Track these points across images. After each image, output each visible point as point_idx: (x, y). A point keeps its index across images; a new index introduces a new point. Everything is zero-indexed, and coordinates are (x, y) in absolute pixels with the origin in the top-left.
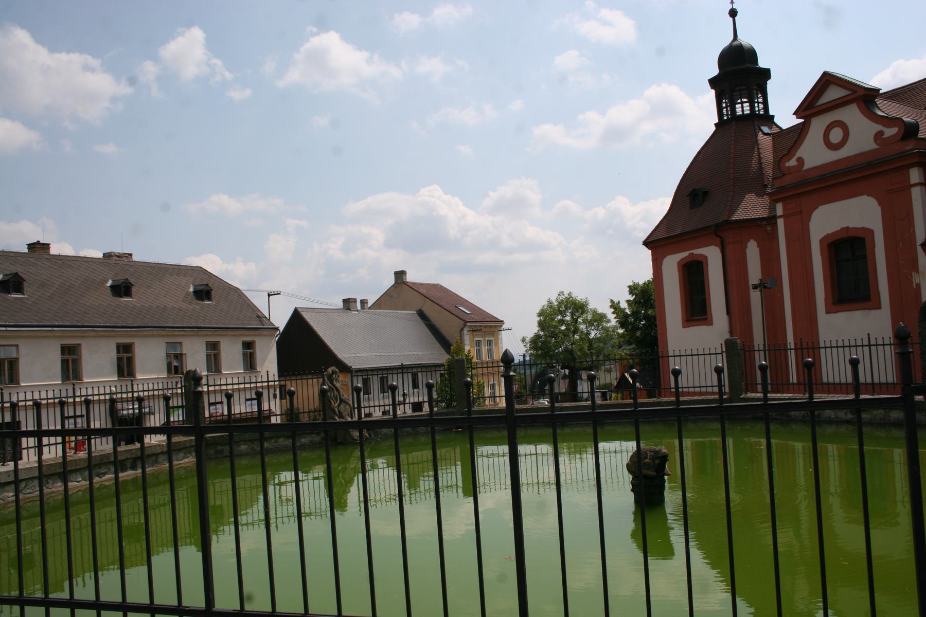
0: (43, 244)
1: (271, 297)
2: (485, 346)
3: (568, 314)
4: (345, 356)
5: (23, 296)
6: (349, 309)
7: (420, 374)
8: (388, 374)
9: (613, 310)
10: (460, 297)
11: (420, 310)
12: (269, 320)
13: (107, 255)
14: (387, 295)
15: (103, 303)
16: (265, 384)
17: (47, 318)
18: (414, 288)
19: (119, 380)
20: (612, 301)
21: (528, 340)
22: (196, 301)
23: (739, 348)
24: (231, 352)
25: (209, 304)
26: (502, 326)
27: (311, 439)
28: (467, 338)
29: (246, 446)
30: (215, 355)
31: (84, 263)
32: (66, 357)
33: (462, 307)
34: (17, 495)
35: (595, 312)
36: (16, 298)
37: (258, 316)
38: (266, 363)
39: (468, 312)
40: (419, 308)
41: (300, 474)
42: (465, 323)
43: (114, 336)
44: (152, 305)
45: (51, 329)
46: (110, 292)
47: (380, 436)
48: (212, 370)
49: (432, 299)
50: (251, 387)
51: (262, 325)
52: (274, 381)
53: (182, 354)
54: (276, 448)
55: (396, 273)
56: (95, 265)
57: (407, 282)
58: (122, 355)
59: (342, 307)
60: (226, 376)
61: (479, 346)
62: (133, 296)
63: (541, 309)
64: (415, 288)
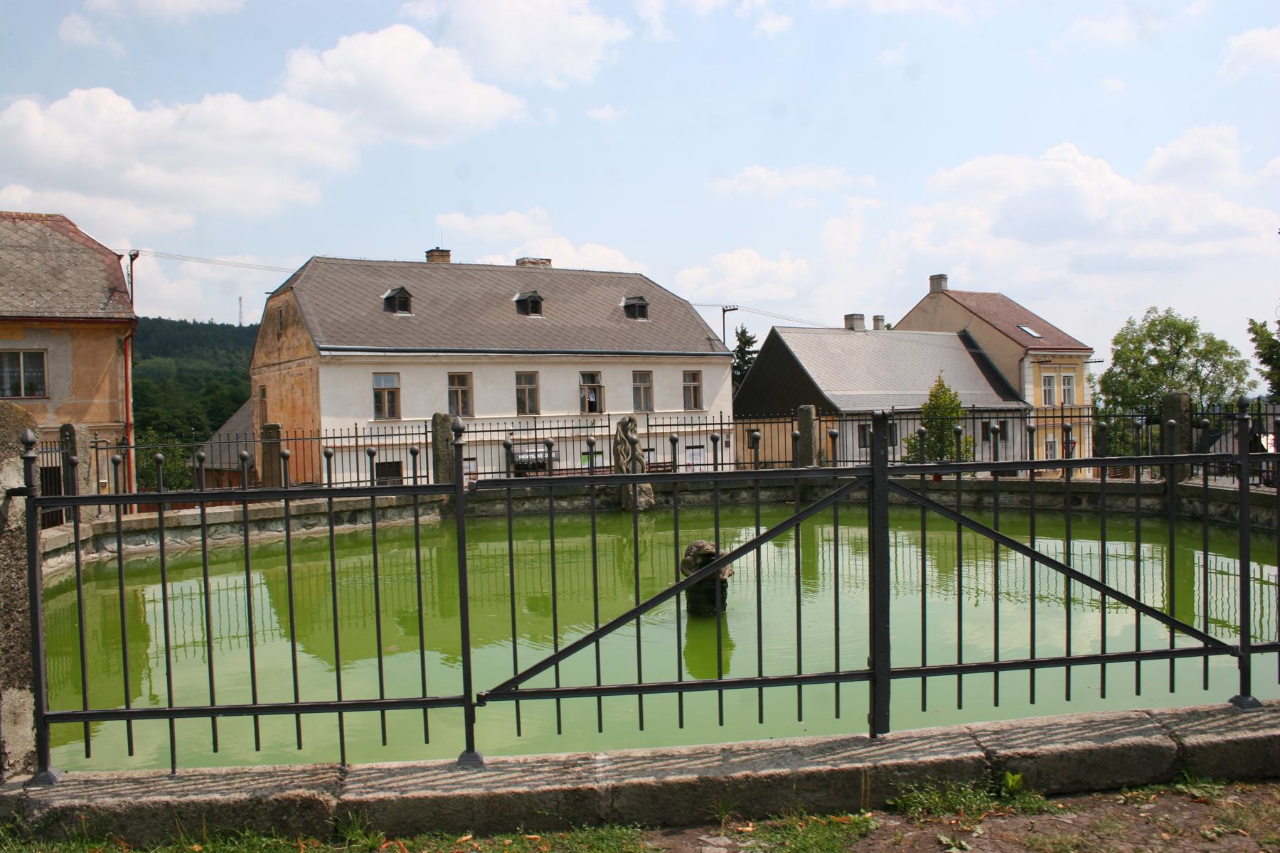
0: (442, 251)
3: (1165, 341)
4: (835, 393)
5: (409, 315)
6: (852, 329)
7: (1010, 421)
8: (990, 418)
9: (1254, 336)
10: (1030, 312)
11: (964, 331)
13: (520, 262)
14: (919, 308)
15: (503, 322)
16: (718, 427)
17: (433, 341)
18: (957, 299)
19: (375, 422)
20: (1252, 322)
21: (1097, 378)
22: (625, 318)
23: (1184, 409)
24: (668, 383)
25: (642, 323)
26: (1090, 356)
28: (1029, 371)
30: (695, 388)
31: (488, 272)
34: (204, 540)
35: (1210, 340)
36: (402, 318)
37: (709, 339)
38: (717, 401)
39: (1035, 334)
41: (1254, 566)
42: (1027, 350)
43: (513, 364)
44: (566, 324)
45: (382, 354)
46: (515, 308)
49: (982, 316)
51: (710, 349)
53: (600, 387)
54: (541, 510)
55: (933, 279)
56: (501, 274)
57: (947, 291)
58: (523, 386)
60: (544, 419)
62: (543, 313)
63: (1119, 334)
64: (958, 300)
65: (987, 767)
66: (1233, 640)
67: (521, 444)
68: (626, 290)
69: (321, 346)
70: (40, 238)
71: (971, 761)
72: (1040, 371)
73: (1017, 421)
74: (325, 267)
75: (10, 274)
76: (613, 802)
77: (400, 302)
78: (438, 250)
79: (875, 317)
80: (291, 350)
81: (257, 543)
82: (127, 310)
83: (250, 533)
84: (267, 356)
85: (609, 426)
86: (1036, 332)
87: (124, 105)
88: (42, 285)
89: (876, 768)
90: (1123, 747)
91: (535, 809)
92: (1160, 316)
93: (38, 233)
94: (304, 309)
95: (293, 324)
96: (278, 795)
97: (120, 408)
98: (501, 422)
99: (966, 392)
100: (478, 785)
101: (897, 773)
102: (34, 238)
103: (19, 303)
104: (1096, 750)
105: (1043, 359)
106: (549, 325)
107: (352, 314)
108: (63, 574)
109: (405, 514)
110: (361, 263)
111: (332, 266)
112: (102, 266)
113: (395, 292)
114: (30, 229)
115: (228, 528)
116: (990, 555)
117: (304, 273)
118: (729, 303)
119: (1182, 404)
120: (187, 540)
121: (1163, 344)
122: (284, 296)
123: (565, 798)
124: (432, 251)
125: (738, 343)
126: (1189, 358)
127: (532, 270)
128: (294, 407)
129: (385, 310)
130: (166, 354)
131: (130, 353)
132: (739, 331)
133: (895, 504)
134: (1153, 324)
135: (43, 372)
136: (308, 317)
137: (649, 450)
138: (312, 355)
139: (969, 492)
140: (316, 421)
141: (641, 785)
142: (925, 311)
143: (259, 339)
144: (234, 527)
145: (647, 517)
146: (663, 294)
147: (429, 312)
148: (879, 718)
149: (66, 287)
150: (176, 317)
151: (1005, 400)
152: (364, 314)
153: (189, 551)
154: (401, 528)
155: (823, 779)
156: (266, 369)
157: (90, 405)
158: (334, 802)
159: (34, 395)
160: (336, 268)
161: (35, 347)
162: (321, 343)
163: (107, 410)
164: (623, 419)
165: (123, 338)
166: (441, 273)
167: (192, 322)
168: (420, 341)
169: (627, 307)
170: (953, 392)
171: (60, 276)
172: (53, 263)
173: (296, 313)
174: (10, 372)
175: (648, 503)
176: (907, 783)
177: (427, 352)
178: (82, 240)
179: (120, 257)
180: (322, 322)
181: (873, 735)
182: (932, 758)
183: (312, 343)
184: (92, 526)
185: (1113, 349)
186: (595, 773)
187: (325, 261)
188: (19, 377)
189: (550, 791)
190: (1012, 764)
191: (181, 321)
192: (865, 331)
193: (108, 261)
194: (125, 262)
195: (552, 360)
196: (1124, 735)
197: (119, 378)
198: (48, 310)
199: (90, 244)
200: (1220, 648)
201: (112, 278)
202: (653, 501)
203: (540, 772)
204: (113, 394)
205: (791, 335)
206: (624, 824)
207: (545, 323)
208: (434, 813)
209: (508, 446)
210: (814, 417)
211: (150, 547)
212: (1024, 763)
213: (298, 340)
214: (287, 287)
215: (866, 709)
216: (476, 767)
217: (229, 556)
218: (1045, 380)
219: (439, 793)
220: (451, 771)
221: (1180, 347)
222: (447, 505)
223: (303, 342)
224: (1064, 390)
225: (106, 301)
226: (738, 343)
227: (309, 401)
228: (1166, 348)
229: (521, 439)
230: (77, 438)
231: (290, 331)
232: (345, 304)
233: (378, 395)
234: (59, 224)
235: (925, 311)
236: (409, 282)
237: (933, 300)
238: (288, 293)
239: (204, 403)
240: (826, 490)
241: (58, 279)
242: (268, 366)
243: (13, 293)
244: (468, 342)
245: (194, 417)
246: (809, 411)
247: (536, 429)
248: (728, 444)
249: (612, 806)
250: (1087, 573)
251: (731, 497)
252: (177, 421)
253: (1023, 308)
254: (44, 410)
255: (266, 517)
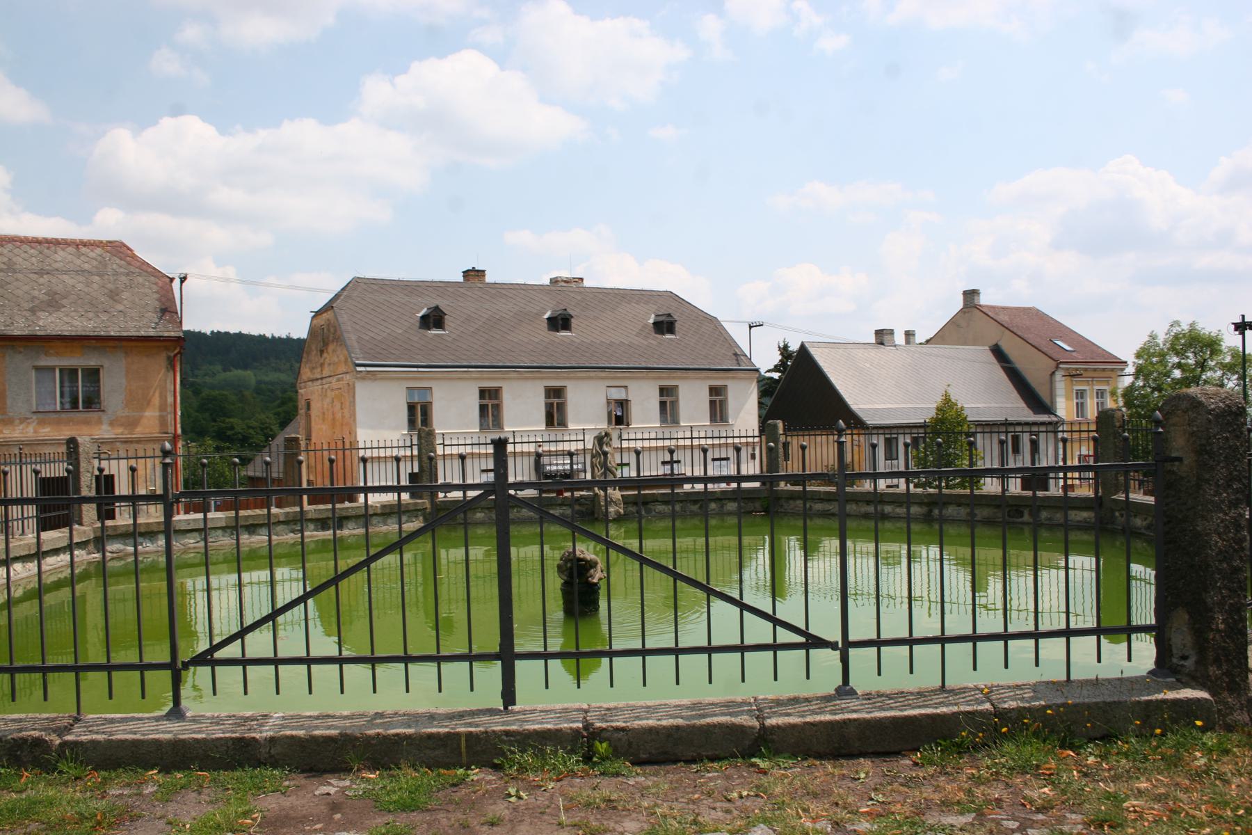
0: (478, 271)
1: (753, 329)
2: (1092, 398)
4: (862, 407)
5: (443, 332)
6: (882, 344)
8: (898, 434)
10: (1064, 326)
12: (750, 359)
14: (953, 322)
15: (533, 339)
17: (464, 357)
18: (990, 314)
19: (546, 430)
22: (654, 334)
23: (1118, 424)
25: (670, 339)
26: (1124, 369)
27: (561, 511)
28: (1061, 384)
29: (483, 514)
31: (520, 291)
32: (714, 398)
33: (1062, 341)
36: (435, 335)
37: (736, 354)
39: (1068, 348)
40: (994, 343)
46: (546, 325)
47: (654, 513)
48: (488, 425)
49: (1015, 330)
50: (720, 444)
51: (740, 365)
52: (754, 437)
54: (518, 518)
56: (534, 293)
57: (980, 306)
59: (874, 342)
61: (1102, 397)
64: (992, 315)
65: (584, 737)
66: (836, 636)
67: (550, 455)
68: (656, 307)
69: (357, 362)
70: (100, 262)
71: (569, 731)
72: (1072, 385)
73: (1051, 435)
74: (365, 287)
75: (72, 296)
76: (270, 749)
77: (434, 320)
78: (474, 270)
79: (906, 331)
80: (332, 366)
81: (247, 546)
82: (176, 329)
83: (241, 537)
84: (311, 371)
85: (584, 440)
86: (1069, 345)
87: (209, 131)
88: (100, 307)
89: (486, 732)
90: (708, 725)
91: (210, 753)
92: (1183, 330)
93: (99, 258)
94: (343, 327)
95: (333, 341)
96: (15, 735)
97: (169, 420)
98: (468, 437)
99: (997, 405)
100: (169, 732)
101: (505, 738)
102: (95, 263)
103: (78, 323)
104: (683, 727)
105: (1074, 373)
106: (578, 341)
107: (389, 331)
108: (62, 571)
109: (389, 521)
110: (400, 283)
111: (372, 286)
112: (155, 288)
113: (430, 311)
114: (92, 254)
115: (220, 532)
116: (1000, 573)
117: (345, 293)
118: (755, 319)
119: (1116, 420)
120: (182, 542)
121: (1188, 357)
122: (325, 314)
123: (233, 744)
124: (468, 271)
125: (780, 357)
126: (1215, 372)
127: (565, 289)
128: (334, 419)
129: (420, 328)
130: (245, 367)
131: (178, 369)
132: (782, 345)
133: (891, 517)
134: (1176, 337)
135: (99, 387)
136: (346, 335)
137: (622, 465)
138: (349, 371)
139: (921, 504)
140: (352, 433)
141: (292, 737)
142: (958, 326)
143: (305, 355)
144: (226, 532)
145: (616, 526)
146: (692, 311)
147: (462, 329)
148: (509, 695)
149: (120, 307)
150: (255, 332)
151: (1035, 413)
152: (400, 331)
153: (182, 553)
154: (386, 534)
155: (441, 739)
156: (310, 383)
157: (141, 417)
158: (58, 742)
159: (91, 408)
160: (376, 287)
161: (92, 363)
162: (358, 359)
163: (157, 422)
164: (600, 433)
165: (172, 354)
166: (476, 292)
167: (270, 337)
168: (453, 357)
169: (655, 324)
170: (959, 406)
171: (116, 298)
172: (110, 286)
173: (335, 331)
174: (69, 387)
175: (617, 513)
176: (510, 746)
177: (458, 368)
178: (138, 264)
179: (172, 280)
180: (359, 339)
181: (506, 708)
182: (537, 727)
183: (349, 360)
184: (94, 528)
185: (1134, 363)
186: (264, 726)
187: (365, 281)
188: (77, 391)
189: (221, 738)
190: (605, 735)
191: (260, 335)
192: (895, 346)
193: (160, 284)
194: (176, 284)
195: (579, 375)
196: (716, 715)
197: (168, 393)
198: (104, 329)
199: (145, 267)
200: (819, 643)
201: (164, 300)
202: (622, 511)
203: (223, 724)
204: (163, 407)
205: (820, 350)
206: (274, 767)
207: (575, 339)
208: (133, 752)
209: (538, 456)
210: (781, 432)
211: (147, 549)
212: (616, 735)
213: (338, 357)
214: (328, 307)
215: (500, 687)
216: (177, 718)
217: (221, 558)
218: (1077, 393)
219: (138, 737)
220: (157, 721)
221: (1205, 360)
222: (430, 514)
223: (342, 358)
224: (1098, 403)
225: (157, 321)
226: (780, 357)
227: (347, 414)
228: (1191, 361)
229: (550, 451)
230: (81, 450)
231: (331, 347)
232: (382, 323)
233: (411, 408)
234: (118, 249)
235: (958, 326)
236: (446, 302)
237: (967, 314)
238: (329, 312)
239: (278, 414)
240: (791, 502)
241: (115, 301)
242: (312, 380)
243: (73, 314)
244: (499, 358)
245: (267, 428)
246: (775, 426)
247: (692, 438)
248: (753, 457)
249: (269, 752)
250: (692, 576)
251: (701, 507)
252: (251, 431)
253: (1057, 322)
254: (100, 422)
255: (256, 522)
